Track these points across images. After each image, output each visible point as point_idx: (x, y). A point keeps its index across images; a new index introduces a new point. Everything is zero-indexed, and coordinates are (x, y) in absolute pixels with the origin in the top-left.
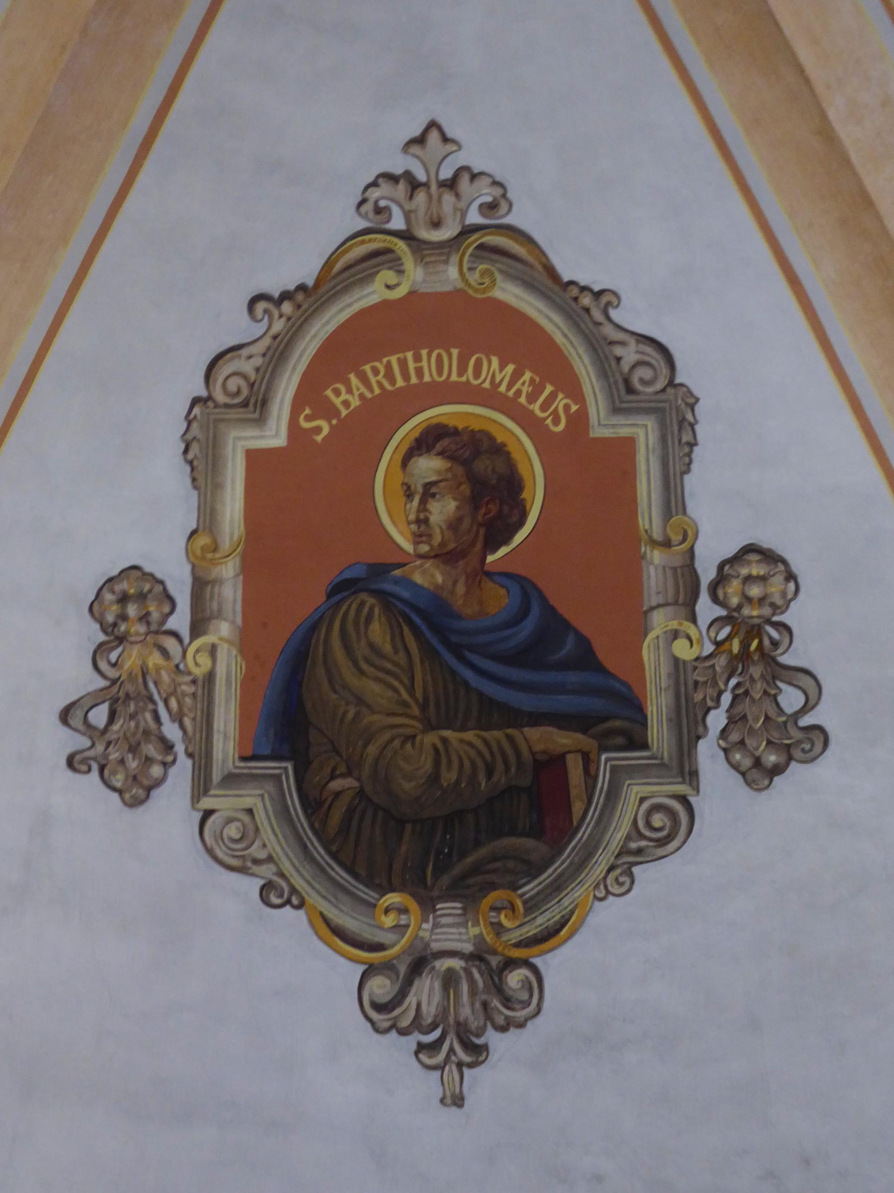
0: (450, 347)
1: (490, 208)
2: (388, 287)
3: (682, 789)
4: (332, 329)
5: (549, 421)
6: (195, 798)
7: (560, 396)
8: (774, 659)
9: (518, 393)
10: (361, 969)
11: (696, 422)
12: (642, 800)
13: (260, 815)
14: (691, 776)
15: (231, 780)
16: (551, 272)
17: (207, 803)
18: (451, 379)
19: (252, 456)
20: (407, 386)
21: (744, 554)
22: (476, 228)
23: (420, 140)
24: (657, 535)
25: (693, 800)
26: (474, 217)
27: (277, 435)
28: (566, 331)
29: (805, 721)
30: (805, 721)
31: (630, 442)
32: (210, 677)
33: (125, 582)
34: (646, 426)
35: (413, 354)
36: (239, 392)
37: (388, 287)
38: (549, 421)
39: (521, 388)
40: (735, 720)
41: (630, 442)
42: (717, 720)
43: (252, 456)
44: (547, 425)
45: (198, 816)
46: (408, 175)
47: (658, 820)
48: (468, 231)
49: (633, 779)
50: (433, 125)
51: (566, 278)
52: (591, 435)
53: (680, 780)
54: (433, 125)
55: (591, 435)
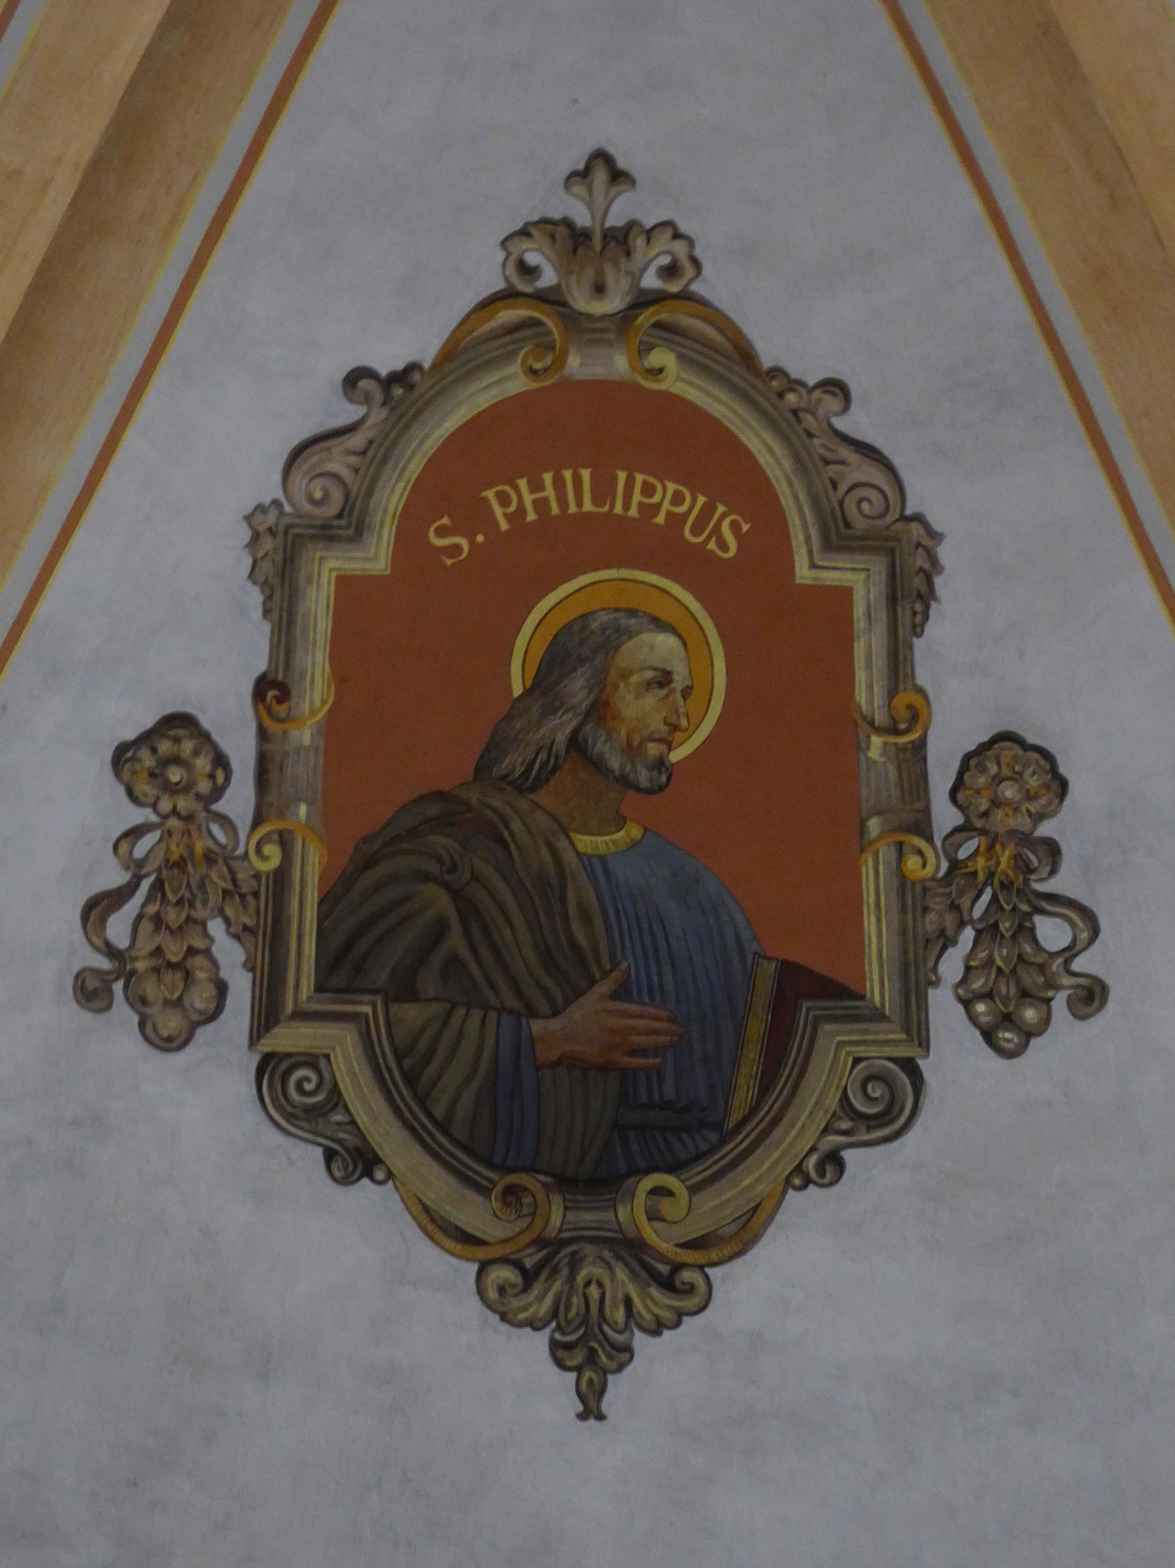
1: (671, 271)
3: (902, 1052)
5: (712, 545)
7: (721, 509)
8: (825, 1164)
10: (474, 1267)
12: (857, 1061)
14: (918, 1033)
16: (745, 354)
19: (345, 583)
20: (579, 513)
21: (984, 751)
22: (658, 298)
23: (582, 175)
24: (880, 718)
25: (921, 1063)
26: (651, 281)
27: (376, 557)
31: (844, 594)
32: (280, 877)
35: (591, 472)
36: (326, 496)
38: (712, 545)
41: (844, 594)
42: (951, 966)
43: (345, 583)
44: (712, 552)
45: (256, 1059)
46: (567, 223)
47: (874, 1090)
48: (643, 300)
50: (601, 157)
51: (767, 363)
52: (663, 523)
53: (904, 1036)
54: (601, 157)
55: (798, 581)
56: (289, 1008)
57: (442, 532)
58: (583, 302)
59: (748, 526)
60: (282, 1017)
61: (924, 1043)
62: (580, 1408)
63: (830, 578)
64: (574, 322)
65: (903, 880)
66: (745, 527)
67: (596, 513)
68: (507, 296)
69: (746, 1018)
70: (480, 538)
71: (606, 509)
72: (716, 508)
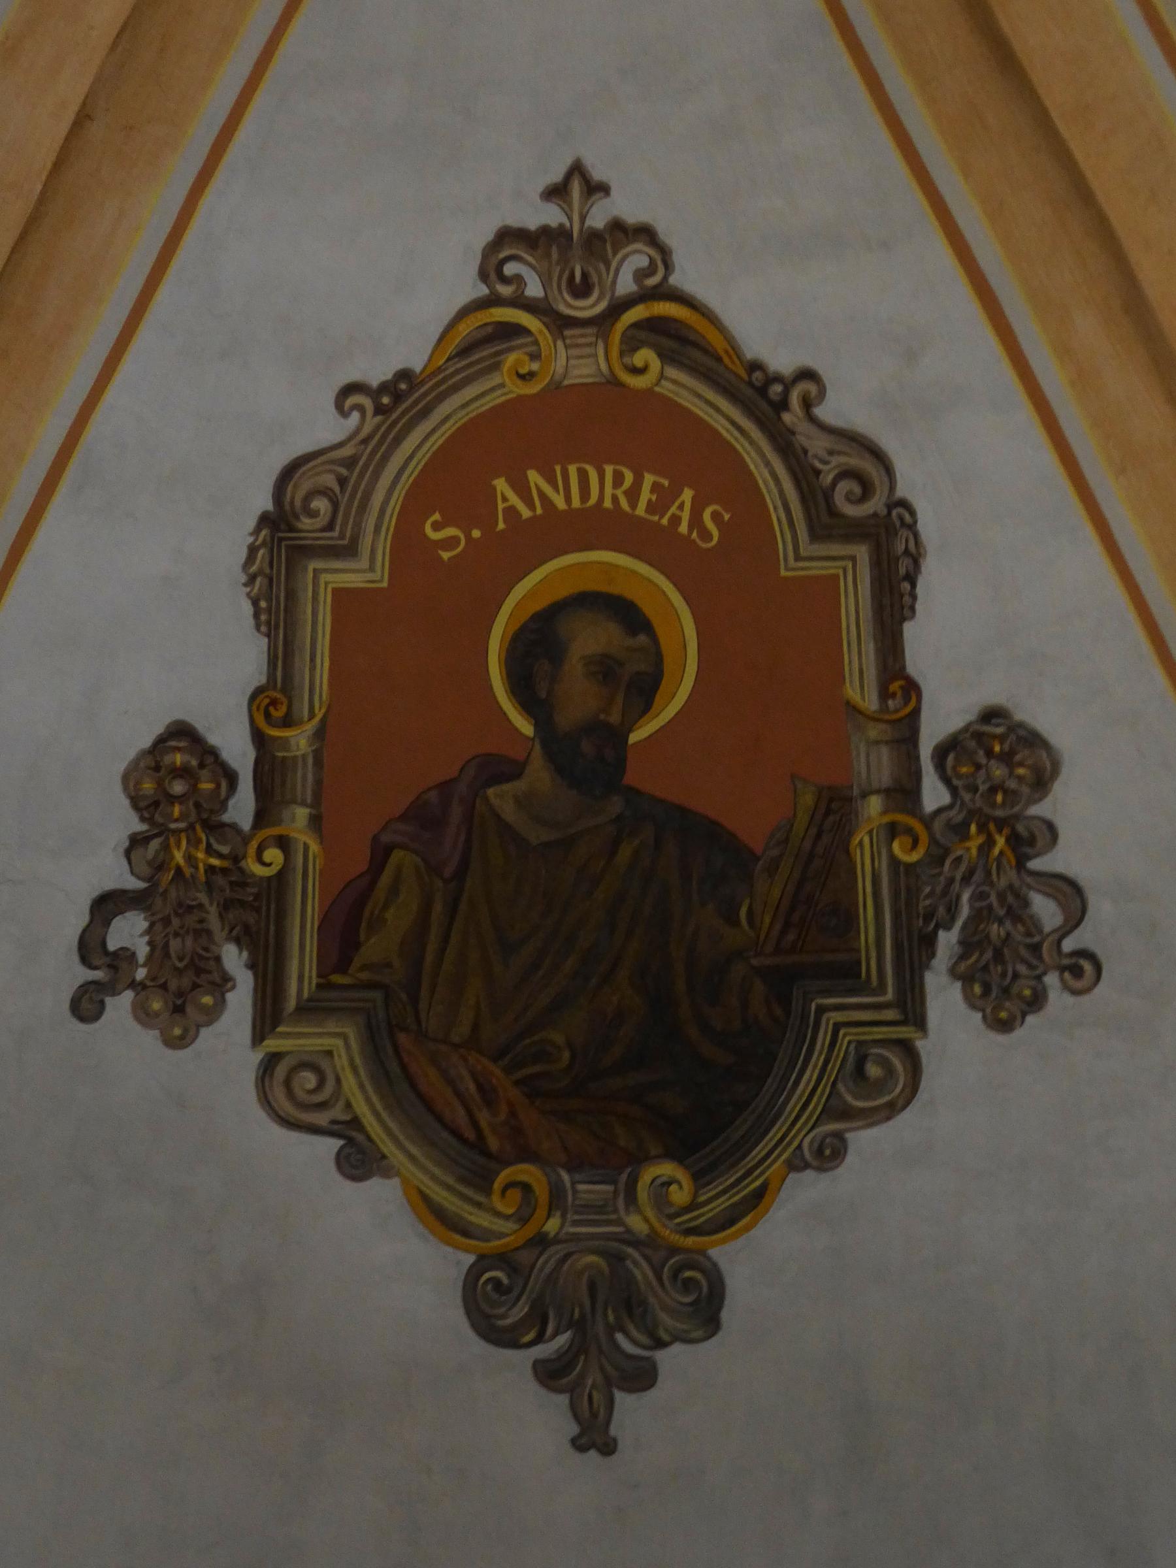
0: (481, 537)
2: (522, 377)
4: (411, 448)
6: (259, 1036)
9: (675, 520)
11: (915, 522)
13: (342, 1061)
15: (308, 1010)
17: (272, 1044)
18: (223, 816)
25: (920, 1044)
28: (358, 1061)
29: (1068, 945)
30: (1068, 945)
33: (178, 763)
34: (853, 559)
37: (522, 377)
39: (678, 513)
40: (968, 946)
42: (947, 941)
45: (257, 1057)
49: (829, 993)
50: (577, 169)
54: (577, 169)
56: (291, 1004)
57: (437, 527)
58: (571, 306)
59: (729, 516)
60: (285, 1014)
61: (920, 1023)
62: (574, 1429)
63: (818, 569)
64: (560, 323)
65: (894, 862)
66: (727, 517)
67: (646, 520)
68: (492, 301)
69: (903, 895)
70: (476, 534)
71: (656, 518)
72: (604, 471)
